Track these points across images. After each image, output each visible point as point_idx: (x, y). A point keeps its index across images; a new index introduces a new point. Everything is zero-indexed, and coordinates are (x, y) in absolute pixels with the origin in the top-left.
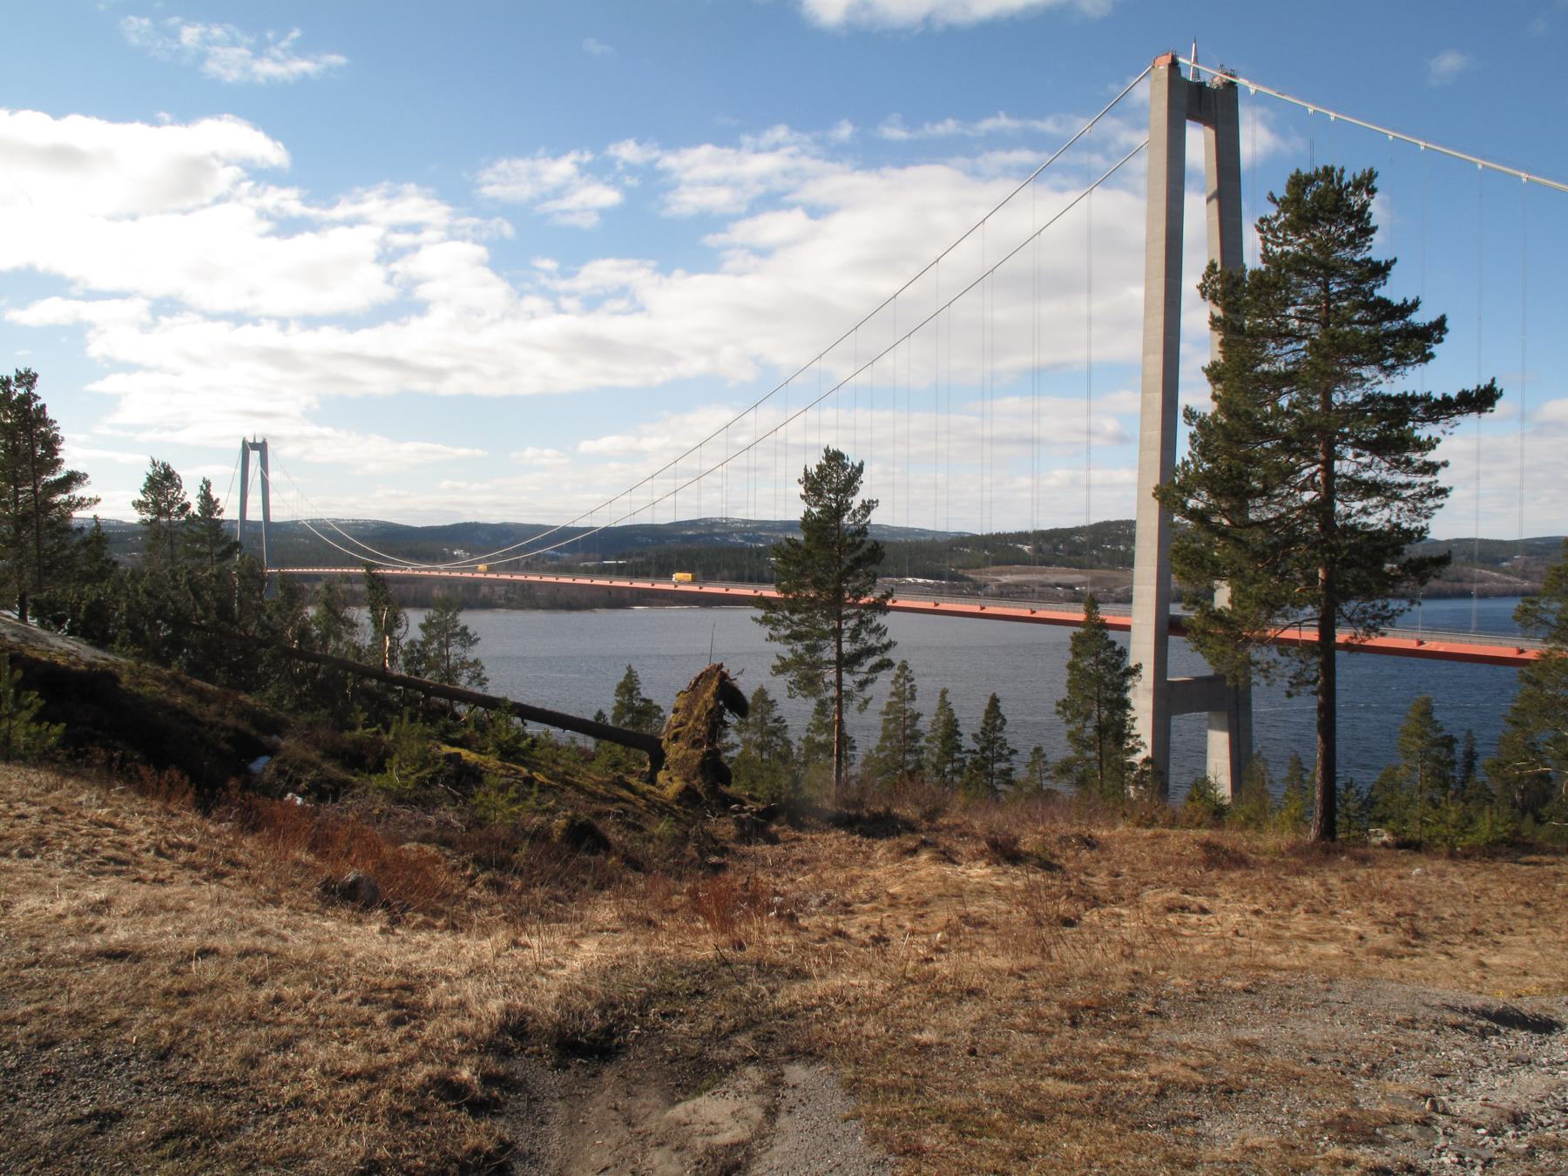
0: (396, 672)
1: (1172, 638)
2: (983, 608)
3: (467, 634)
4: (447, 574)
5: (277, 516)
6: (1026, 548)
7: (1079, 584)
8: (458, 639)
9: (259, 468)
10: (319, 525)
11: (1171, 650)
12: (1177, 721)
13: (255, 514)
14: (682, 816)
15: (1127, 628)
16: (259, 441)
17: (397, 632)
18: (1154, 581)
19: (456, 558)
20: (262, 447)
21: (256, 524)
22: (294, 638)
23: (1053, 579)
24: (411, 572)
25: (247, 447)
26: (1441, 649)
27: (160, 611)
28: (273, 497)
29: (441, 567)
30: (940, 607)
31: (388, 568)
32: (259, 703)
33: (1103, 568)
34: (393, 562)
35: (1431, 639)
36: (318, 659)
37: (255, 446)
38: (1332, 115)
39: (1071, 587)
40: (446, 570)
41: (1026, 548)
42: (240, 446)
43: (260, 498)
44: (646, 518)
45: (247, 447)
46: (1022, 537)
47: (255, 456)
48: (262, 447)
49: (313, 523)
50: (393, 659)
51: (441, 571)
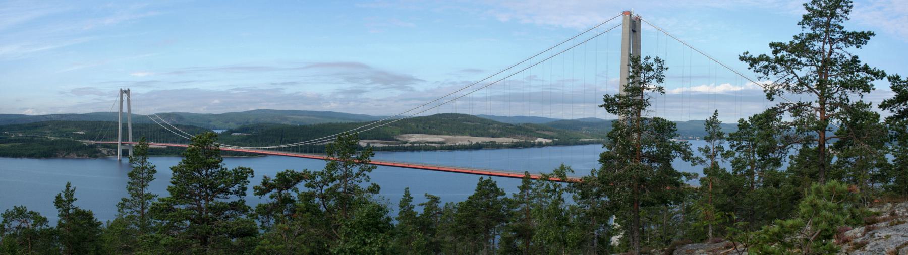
13: (125, 110)
16: (126, 89)
20: (127, 92)
37: (125, 92)
45: (122, 92)
47: (125, 96)
48: (127, 92)
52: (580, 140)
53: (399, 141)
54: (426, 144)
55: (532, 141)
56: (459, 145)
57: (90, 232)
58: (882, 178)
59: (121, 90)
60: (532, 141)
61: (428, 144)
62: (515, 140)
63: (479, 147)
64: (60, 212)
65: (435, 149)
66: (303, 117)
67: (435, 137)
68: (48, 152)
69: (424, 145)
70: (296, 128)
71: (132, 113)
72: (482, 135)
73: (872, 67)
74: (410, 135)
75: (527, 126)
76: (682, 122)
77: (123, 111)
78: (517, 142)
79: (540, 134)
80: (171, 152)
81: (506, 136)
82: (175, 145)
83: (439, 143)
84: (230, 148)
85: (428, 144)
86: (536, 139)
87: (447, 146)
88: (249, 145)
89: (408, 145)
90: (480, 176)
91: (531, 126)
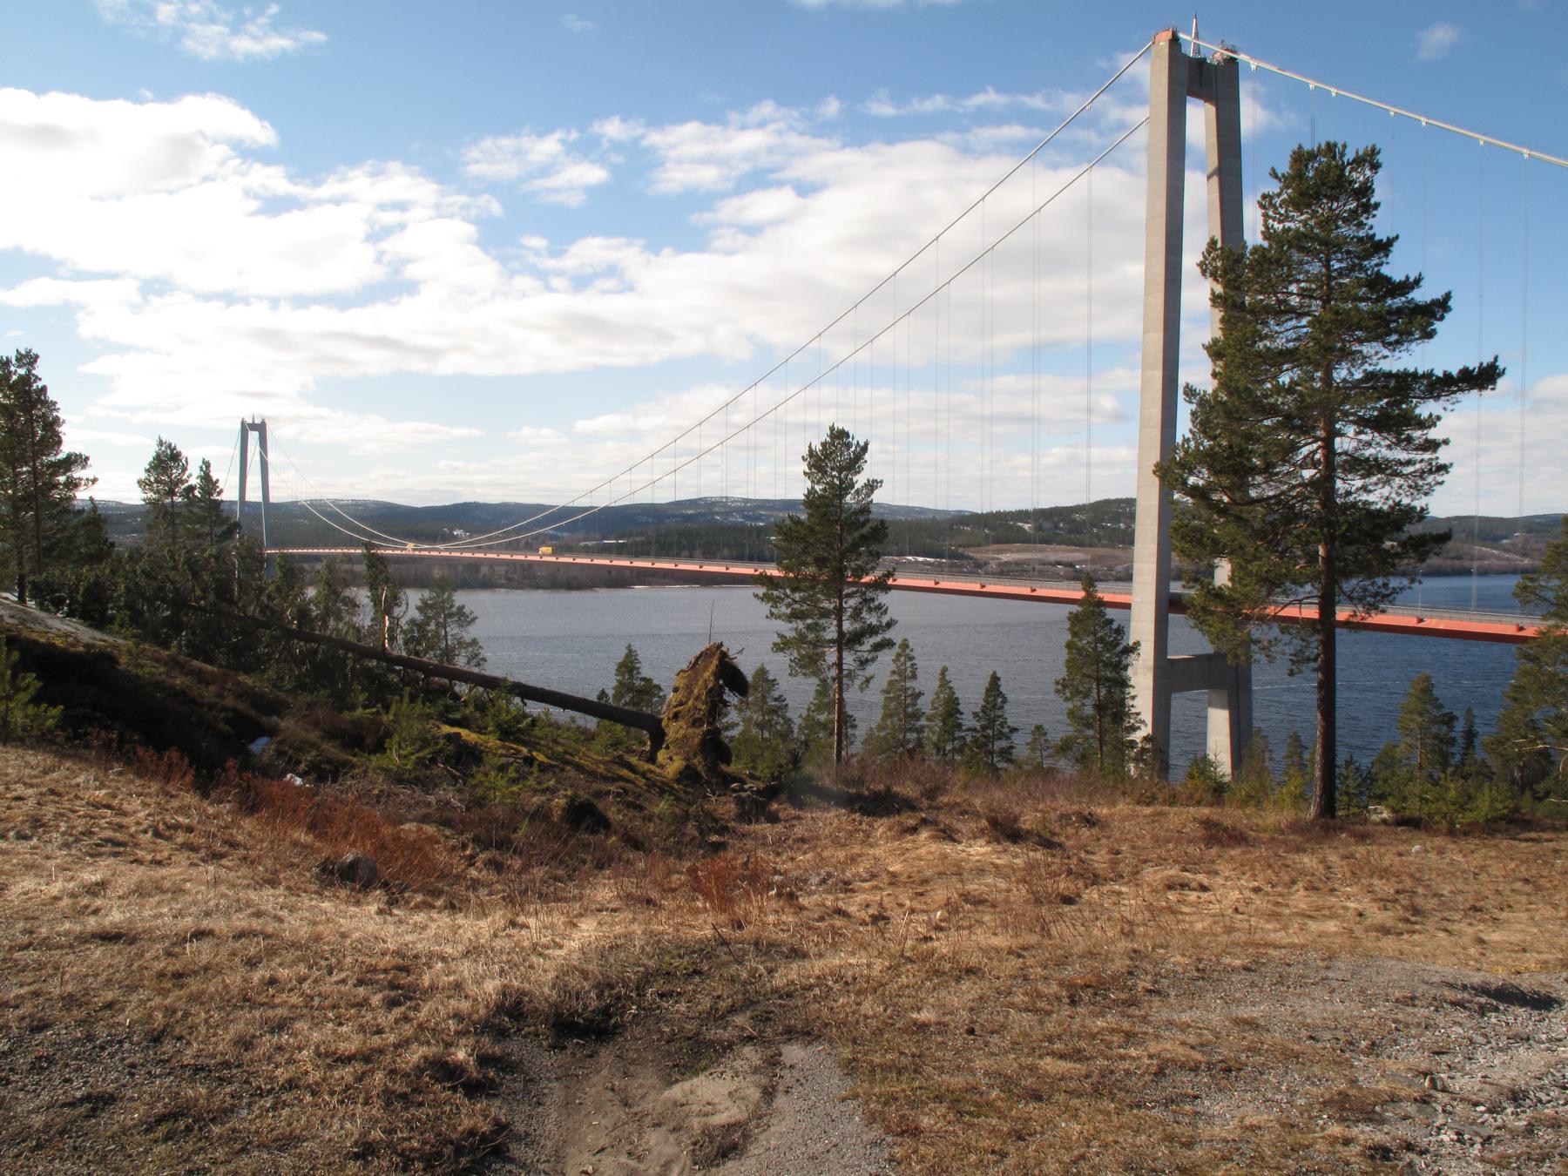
0: (395, 653)
2: (983, 587)
3: (463, 614)
4: (447, 554)
5: (276, 497)
6: (1026, 526)
7: (1080, 563)
8: (456, 618)
9: (258, 448)
10: (319, 505)
13: (255, 495)
16: (258, 421)
17: (397, 611)
19: (456, 538)
20: (261, 428)
21: (256, 505)
22: (293, 619)
23: (1053, 557)
25: (246, 428)
28: (272, 477)
29: (441, 547)
31: (389, 548)
32: (258, 684)
33: (1103, 546)
36: (318, 640)
37: (254, 427)
38: (1334, 91)
39: (1071, 565)
40: (446, 550)
41: (1026, 526)
43: (259, 478)
45: (246, 428)
46: (1022, 515)
47: (254, 436)
48: (261, 428)
49: (313, 503)
50: (392, 639)
51: (441, 551)
52: (475, 432)
58: (960, 751)
59: (243, 423)
67: (1072, 551)
68: (565, 707)
70: (934, 522)
71: (272, 500)
73: (330, 207)
77: (272, 500)
80: (185, 940)
82: (1547, 157)
84: (669, 565)
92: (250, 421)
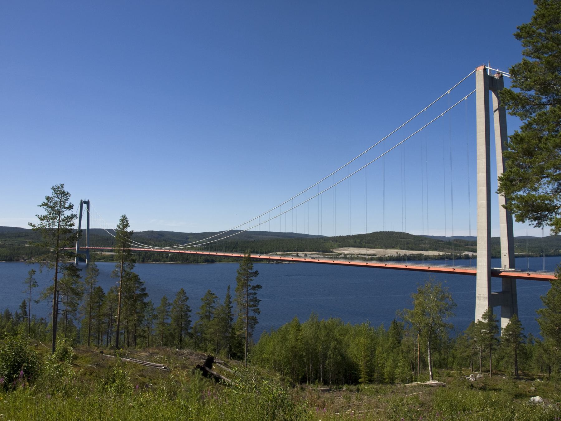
1: (492, 278)
11: (492, 281)
12: (495, 308)
13: (84, 227)
14: (218, 349)
15: (475, 274)
16: (87, 200)
18: (486, 257)
20: (88, 203)
24: (152, 250)
26: (541, 277)
27: (103, 303)
30: (306, 260)
34: (143, 246)
35: (432, 267)
37: (85, 202)
42: (80, 202)
44: (174, 231)
45: (82, 203)
47: (85, 206)
53: (334, 253)
54: (358, 255)
55: (458, 254)
56: (388, 257)
57: (153, 414)
60: (458, 254)
61: (359, 256)
62: (441, 253)
63: (316, 254)
64: (536, 96)
65: (507, 272)
66: (267, 237)
69: (356, 256)
72: (412, 249)
74: (346, 248)
75: (457, 241)
76: (544, 237)
78: (443, 255)
79: (469, 248)
81: (435, 250)
83: (370, 255)
85: (359, 256)
86: (463, 253)
87: (377, 257)
88: (394, 235)
89: (342, 256)
90: (78, 216)
91: (276, 254)
92: (84, 201)
